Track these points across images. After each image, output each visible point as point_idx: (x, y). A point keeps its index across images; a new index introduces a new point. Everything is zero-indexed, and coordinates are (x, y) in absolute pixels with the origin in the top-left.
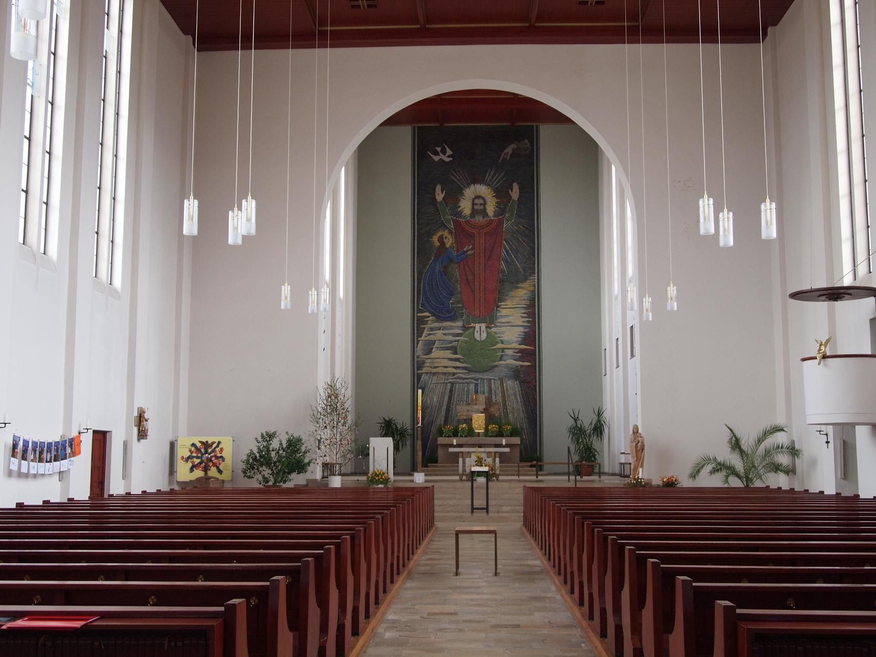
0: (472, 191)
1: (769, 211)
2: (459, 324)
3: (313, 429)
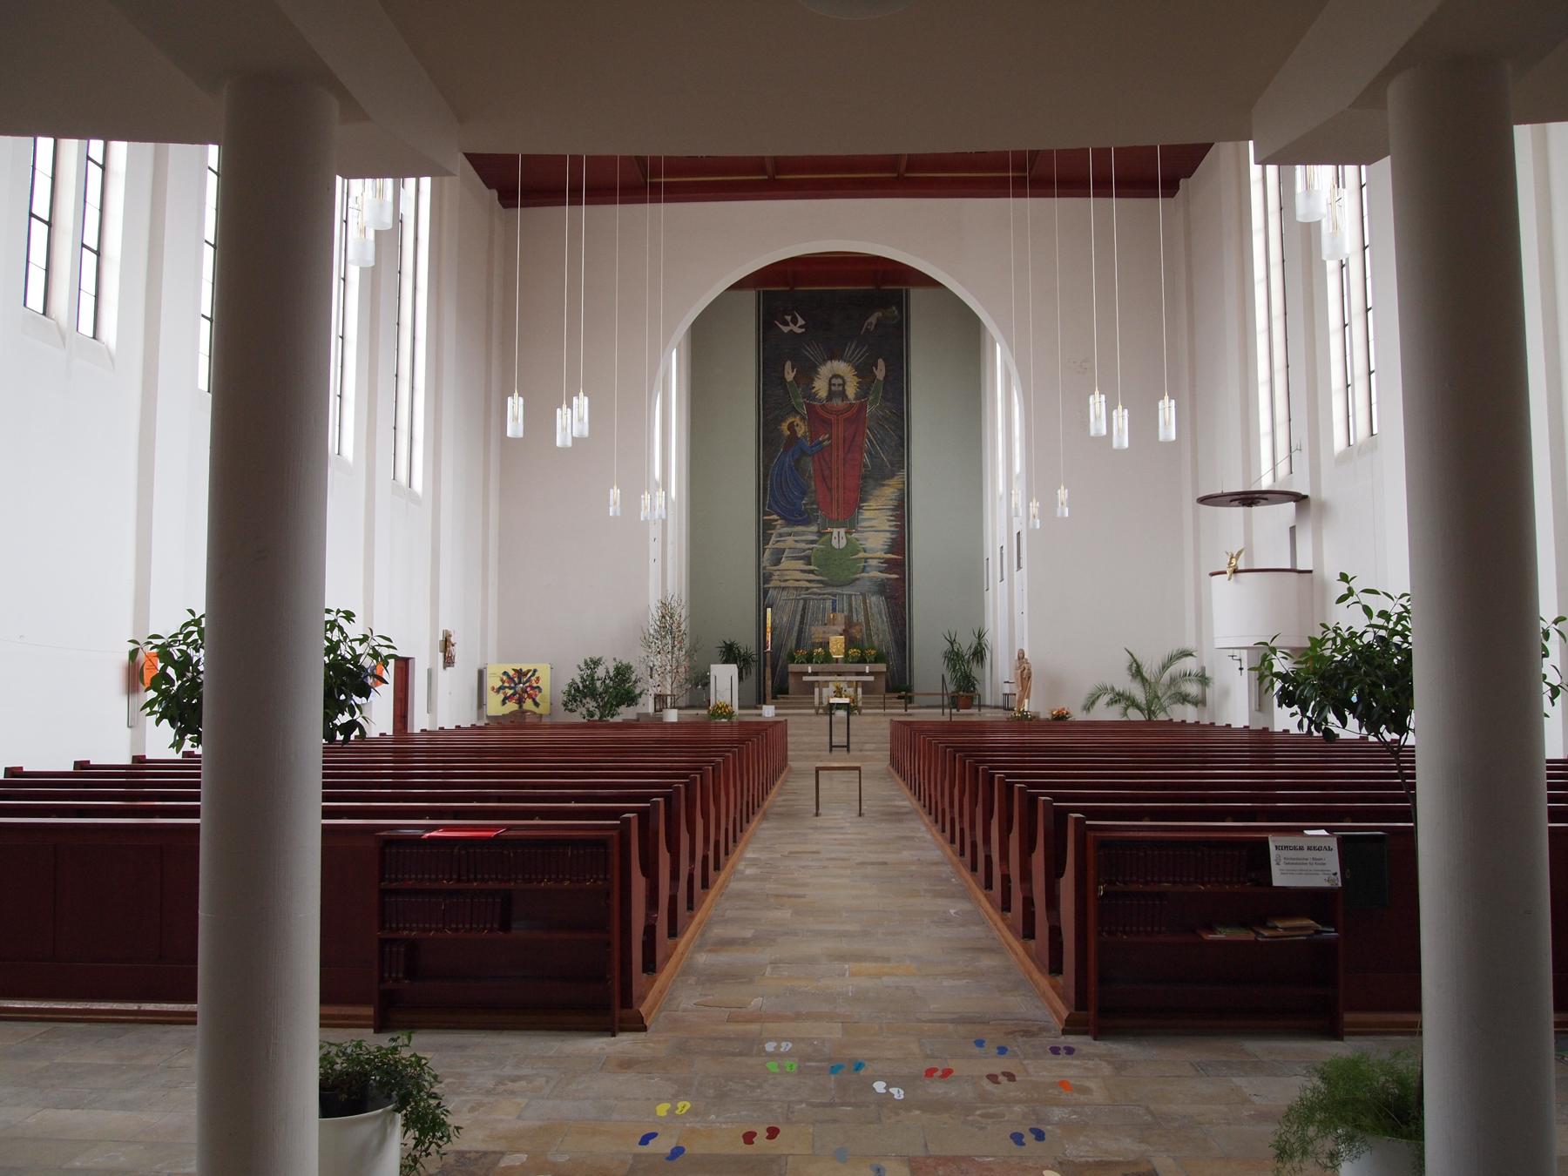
0: (827, 370)
1: (1167, 410)
2: (814, 528)
3: (644, 654)
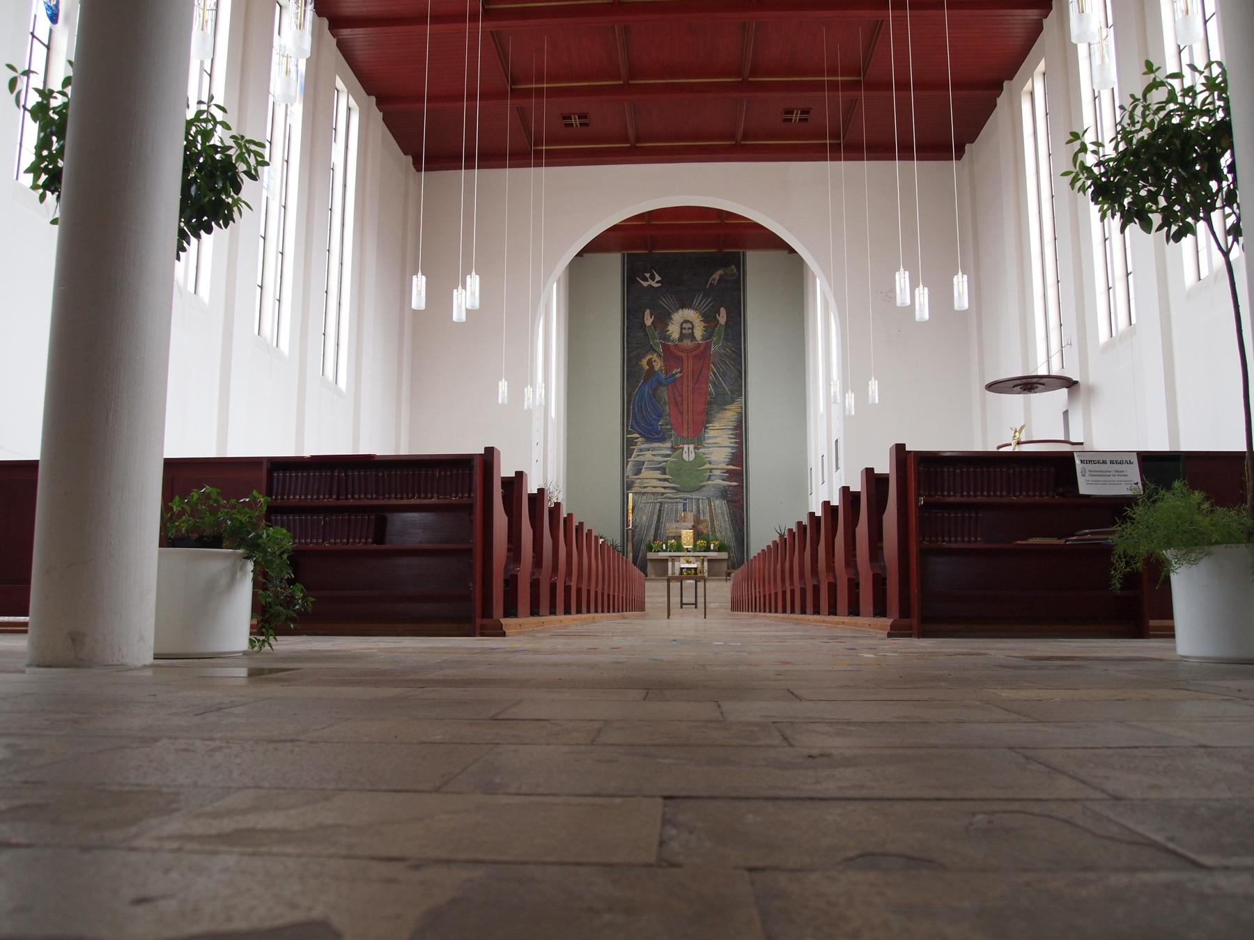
0: (680, 316)
1: (961, 284)
2: (668, 445)
